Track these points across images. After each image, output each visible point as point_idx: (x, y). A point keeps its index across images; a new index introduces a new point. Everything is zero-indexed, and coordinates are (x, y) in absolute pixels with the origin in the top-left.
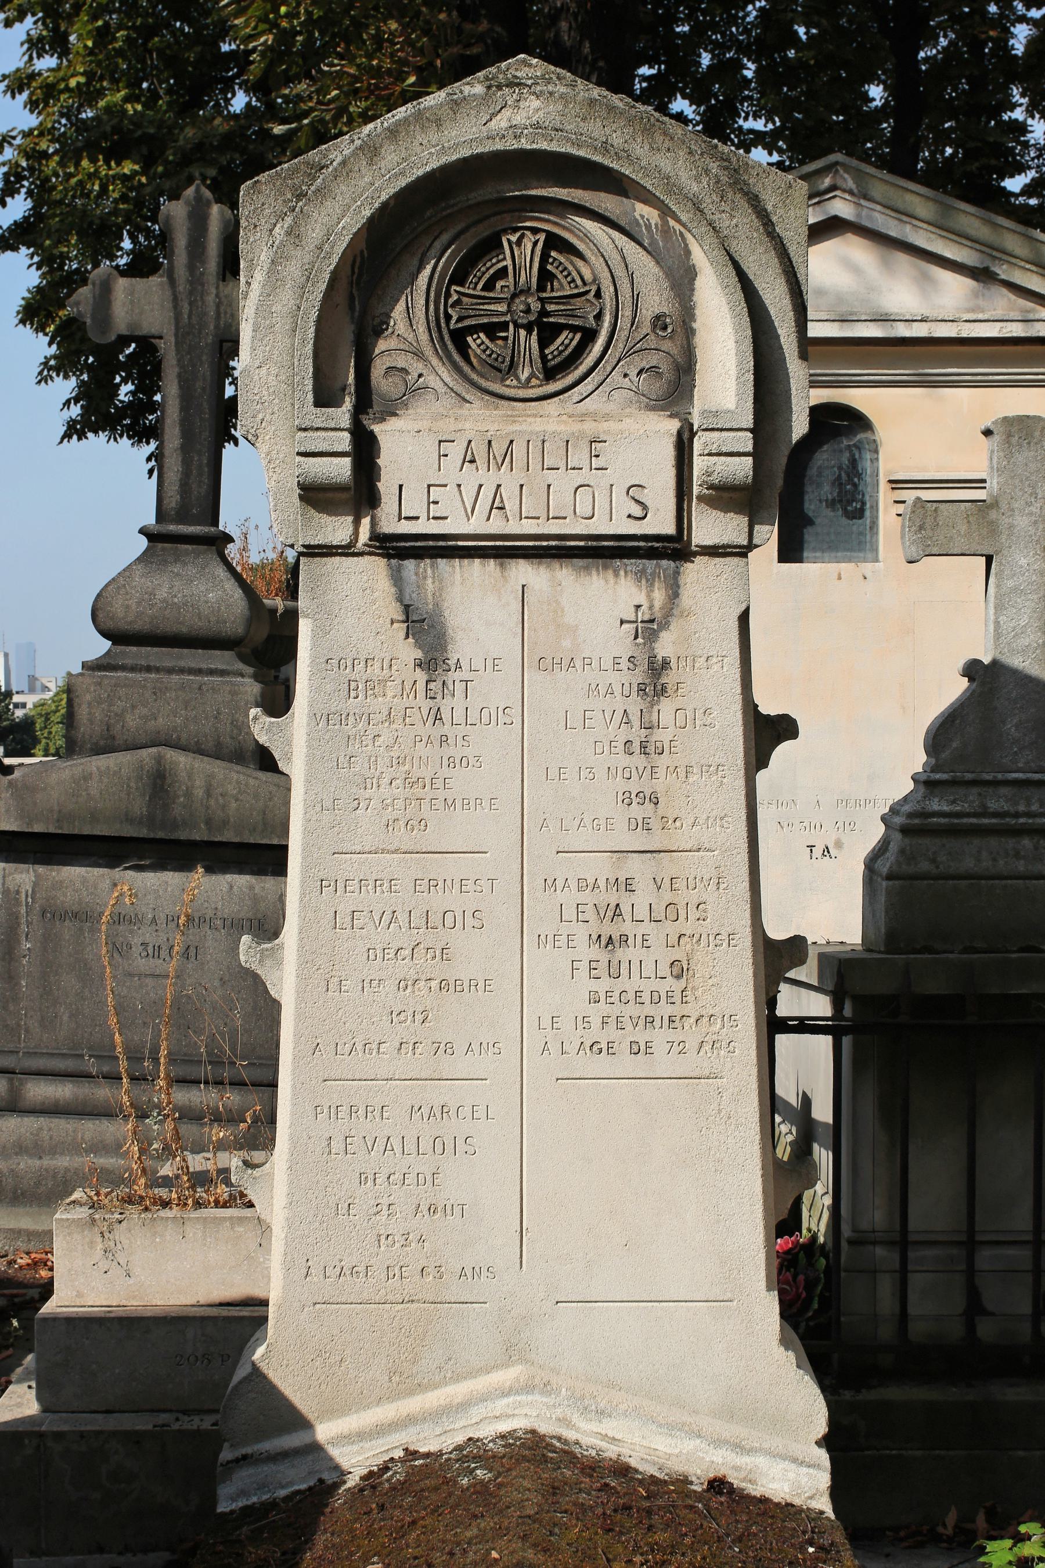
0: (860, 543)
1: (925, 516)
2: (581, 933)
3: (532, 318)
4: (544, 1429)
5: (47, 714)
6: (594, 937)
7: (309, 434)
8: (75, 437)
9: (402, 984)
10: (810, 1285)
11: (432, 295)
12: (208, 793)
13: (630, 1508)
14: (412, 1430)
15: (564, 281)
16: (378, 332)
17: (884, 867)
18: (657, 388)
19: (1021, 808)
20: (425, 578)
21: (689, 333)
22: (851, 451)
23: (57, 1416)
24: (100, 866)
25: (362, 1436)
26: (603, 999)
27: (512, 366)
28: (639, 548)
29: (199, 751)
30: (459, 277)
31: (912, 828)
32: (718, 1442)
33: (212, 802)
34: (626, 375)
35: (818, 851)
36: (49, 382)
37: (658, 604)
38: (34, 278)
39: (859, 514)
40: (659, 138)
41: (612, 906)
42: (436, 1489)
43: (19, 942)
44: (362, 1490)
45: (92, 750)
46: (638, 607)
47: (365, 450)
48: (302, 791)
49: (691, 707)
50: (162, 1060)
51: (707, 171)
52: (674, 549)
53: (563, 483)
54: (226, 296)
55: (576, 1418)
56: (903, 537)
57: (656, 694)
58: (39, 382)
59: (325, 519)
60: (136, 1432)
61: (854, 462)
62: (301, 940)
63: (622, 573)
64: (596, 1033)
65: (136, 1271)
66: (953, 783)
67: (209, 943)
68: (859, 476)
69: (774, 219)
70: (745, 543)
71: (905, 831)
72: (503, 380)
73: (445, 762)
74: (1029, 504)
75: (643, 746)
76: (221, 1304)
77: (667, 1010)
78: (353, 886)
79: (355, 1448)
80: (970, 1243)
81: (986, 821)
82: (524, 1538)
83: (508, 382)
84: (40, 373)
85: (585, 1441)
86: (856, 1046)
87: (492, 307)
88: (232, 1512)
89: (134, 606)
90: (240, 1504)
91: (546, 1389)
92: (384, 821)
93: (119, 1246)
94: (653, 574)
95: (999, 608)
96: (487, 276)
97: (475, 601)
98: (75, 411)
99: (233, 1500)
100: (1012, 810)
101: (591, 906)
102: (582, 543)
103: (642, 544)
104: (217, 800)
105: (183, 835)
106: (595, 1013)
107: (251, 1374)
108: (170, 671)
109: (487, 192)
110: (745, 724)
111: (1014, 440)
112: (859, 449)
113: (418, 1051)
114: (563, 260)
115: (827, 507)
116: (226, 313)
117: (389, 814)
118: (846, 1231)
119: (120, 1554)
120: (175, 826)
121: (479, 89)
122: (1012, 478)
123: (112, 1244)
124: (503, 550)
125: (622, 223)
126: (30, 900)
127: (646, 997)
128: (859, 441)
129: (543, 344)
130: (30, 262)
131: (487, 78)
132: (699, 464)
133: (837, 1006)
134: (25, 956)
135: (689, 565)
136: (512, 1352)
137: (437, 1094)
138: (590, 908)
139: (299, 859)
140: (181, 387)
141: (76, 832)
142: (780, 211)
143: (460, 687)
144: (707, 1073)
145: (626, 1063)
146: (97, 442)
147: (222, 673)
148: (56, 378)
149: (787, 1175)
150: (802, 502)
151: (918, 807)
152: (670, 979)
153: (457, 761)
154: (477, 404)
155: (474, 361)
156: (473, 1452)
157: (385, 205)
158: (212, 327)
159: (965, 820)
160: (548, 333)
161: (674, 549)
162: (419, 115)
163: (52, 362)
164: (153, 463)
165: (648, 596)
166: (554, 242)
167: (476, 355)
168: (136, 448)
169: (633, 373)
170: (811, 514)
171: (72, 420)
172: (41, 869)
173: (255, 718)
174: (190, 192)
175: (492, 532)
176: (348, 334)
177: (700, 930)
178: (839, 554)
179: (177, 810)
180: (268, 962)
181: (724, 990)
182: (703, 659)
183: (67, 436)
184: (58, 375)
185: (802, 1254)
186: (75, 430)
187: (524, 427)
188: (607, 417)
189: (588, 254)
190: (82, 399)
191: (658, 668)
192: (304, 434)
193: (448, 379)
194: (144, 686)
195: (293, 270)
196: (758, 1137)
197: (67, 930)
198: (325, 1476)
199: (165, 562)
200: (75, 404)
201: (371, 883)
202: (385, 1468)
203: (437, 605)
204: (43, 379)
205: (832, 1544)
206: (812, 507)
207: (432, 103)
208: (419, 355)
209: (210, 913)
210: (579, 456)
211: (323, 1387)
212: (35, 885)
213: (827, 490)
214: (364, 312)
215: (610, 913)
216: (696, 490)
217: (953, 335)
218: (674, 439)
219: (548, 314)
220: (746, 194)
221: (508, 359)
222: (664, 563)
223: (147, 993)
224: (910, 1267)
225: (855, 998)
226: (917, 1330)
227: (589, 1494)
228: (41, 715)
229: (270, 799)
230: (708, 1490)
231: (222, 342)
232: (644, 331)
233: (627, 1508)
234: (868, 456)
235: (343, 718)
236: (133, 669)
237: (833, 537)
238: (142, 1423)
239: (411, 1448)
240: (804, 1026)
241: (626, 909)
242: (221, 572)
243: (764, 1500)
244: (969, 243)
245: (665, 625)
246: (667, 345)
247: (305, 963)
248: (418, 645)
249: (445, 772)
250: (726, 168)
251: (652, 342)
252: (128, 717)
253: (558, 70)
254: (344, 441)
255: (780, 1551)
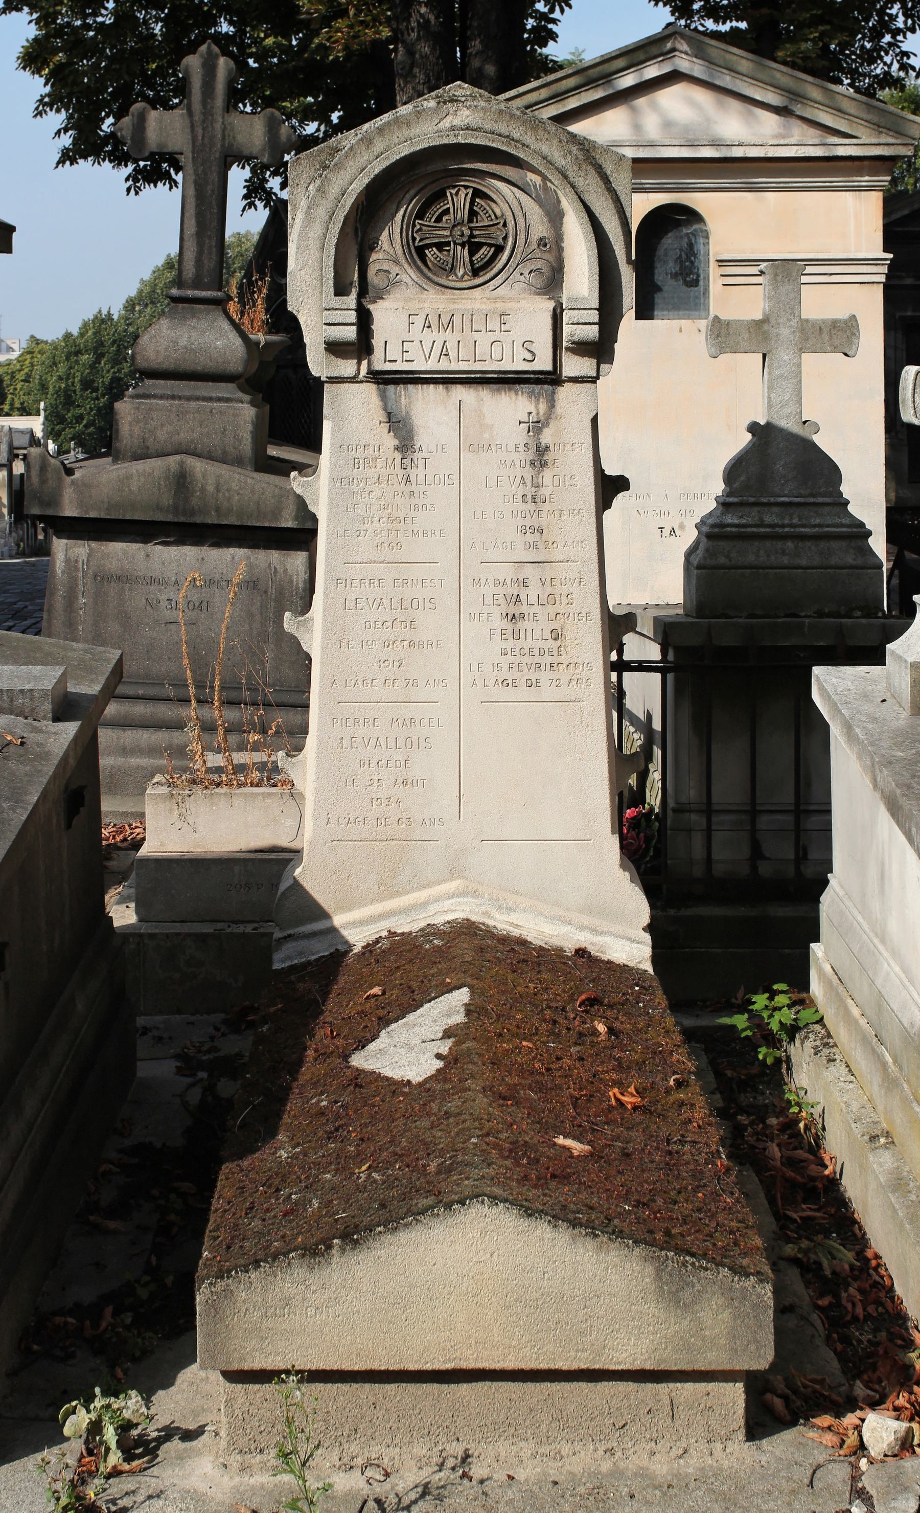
0: (696, 305)
1: (721, 328)
2: (496, 612)
3: (465, 240)
4: (473, 918)
5: (13, 373)
6: (504, 615)
7: (332, 312)
8: (68, 163)
9: (387, 643)
10: (648, 840)
11: (405, 226)
12: (218, 489)
13: (527, 961)
14: (393, 919)
15: (484, 216)
16: (372, 249)
17: (695, 561)
18: (539, 282)
19: (786, 522)
20: (400, 396)
21: (560, 250)
22: (689, 238)
23: (149, 924)
24: (137, 542)
25: (361, 923)
26: (509, 653)
27: (453, 267)
28: (530, 378)
29: (209, 456)
30: (420, 215)
31: (713, 533)
32: (582, 928)
33: (221, 495)
34: (522, 274)
35: (666, 532)
36: (44, 115)
37: (542, 412)
38: (32, 32)
39: (696, 283)
40: (541, 132)
41: (515, 596)
42: (409, 951)
43: (77, 598)
44: (363, 953)
45: (132, 456)
46: (530, 413)
47: (364, 320)
48: (325, 525)
49: (562, 474)
50: (216, 688)
51: (570, 152)
52: (552, 379)
53: (484, 340)
54: (230, 124)
55: (494, 912)
56: (707, 340)
57: (541, 466)
58: (35, 116)
59: (340, 361)
60: (203, 934)
61: (691, 246)
62: (324, 616)
63: (520, 393)
64: (505, 674)
65: (200, 828)
66: (741, 504)
67: (217, 599)
68: (695, 255)
69: (611, 179)
70: (595, 375)
71: (709, 536)
72: (447, 276)
73: (412, 508)
74: (789, 320)
75: (534, 498)
76: (256, 851)
77: (549, 660)
78: (356, 583)
79: (358, 930)
80: (753, 812)
81: (763, 530)
82: (465, 972)
83: (450, 278)
84: (37, 108)
85: (499, 926)
86: (677, 681)
87: (440, 232)
88: (283, 969)
89: (162, 351)
90: (287, 964)
91: (475, 894)
92: (375, 543)
93: (189, 812)
94: (539, 394)
95: (771, 388)
96: (437, 213)
97: (429, 409)
98: (66, 140)
99: (283, 962)
100: (780, 523)
101: (502, 595)
102: (496, 376)
103: (532, 376)
104: (224, 494)
105: (198, 520)
106: (505, 661)
107: (293, 884)
108: (189, 399)
109: (437, 166)
110: (595, 481)
111: (779, 278)
112: (695, 236)
113: (396, 685)
114: (483, 204)
115: (672, 278)
116: (229, 136)
117: (378, 539)
118: (671, 803)
119: (192, 1014)
120: (193, 513)
121: (432, 104)
122: (778, 303)
123: (184, 810)
124: (448, 380)
125: (519, 184)
126: (85, 567)
127: (536, 652)
128: (695, 230)
129: (471, 254)
130: (30, 18)
131: (437, 97)
132: (567, 330)
133: (664, 652)
134: (81, 609)
135: (560, 388)
136: (454, 872)
137: (408, 711)
138: (501, 597)
139: (323, 566)
140: (196, 190)
141: (121, 517)
142: (615, 175)
143: (421, 462)
144: (573, 698)
145: (524, 693)
146: (85, 166)
147: (228, 400)
148: (49, 112)
149: (626, 766)
150: (653, 274)
151: (718, 521)
152: (550, 640)
153: (420, 507)
154: (432, 291)
155: (430, 264)
156: (430, 931)
157: (376, 176)
158: (219, 146)
159: (749, 530)
160: (474, 248)
161: (552, 379)
162: (397, 120)
163: (47, 99)
164: (130, 182)
165: (536, 407)
166: (477, 193)
167: (431, 261)
168: (116, 170)
169: (526, 272)
170: (659, 283)
171: (65, 148)
172: (94, 544)
173: (294, 478)
174: (203, 48)
175: (441, 369)
176: (354, 251)
177: (569, 610)
178: (681, 313)
179: (195, 501)
180: (302, 629)
181: (584, 647)
182: (569, 445)
183: (61, 162)
184: (51, 110)
185: (643, 820)
186: (68, 157)
187: (460, 306)
188: (510, 299)
189: (498, 201)
190: (71, 129)
191: (542, 450)
192: (328, 312)
193: (414, 277)
194: (170, 410)
195: (321, 212)
196: (605, 738)
197: (112, 589)
198: (340, 947)
199: (184, 318)
200: (65, 133)
201: (367, 581)
202: (377, 941)
203: (407, 412)
204: (39, 113)
205: (650, 986)
206: (661, 278)
207: (405, 112)
208: (396, 262)
209: (218, 577)
210: (494, 324)
211: (338, 893)
212: (89, 555)
213: (672, 267)
214: (362, 239)
215: (514, 600)
216: (565, 344)
217: (762, 155)
218: (551, 313)
219: (475, 237)
220: (594, 165)
221: (450, 264)
222: (546, 386)
223: (171, 636)
224: (713, 827)
225: (676, 649)
226: (719, 870)
227: (502, 953)
228: (7, 373)
229: (263, 493)
230: (574, 955)
231: (226, 157)
232: (533, 248)
233: (524, 961)
234: (701, 240)
235: (350, 481)
236: (161, 397)
237: (676, 300)
238: (207, 929)
239: (392, 930)
240: (642, 667)
241: (523, 597)
242: (225, 325)
243: (609, 962)
244: (772, 89)
245: (546, 424)
246: (547, 256)
247: (327, 629)
248: (396, 436)
249: (412, 513)
250: (582, 150)
251: (538, 253)
252: (159, 433)
253: (480, 91)
254: (352, 316)
255: (618, 988)
